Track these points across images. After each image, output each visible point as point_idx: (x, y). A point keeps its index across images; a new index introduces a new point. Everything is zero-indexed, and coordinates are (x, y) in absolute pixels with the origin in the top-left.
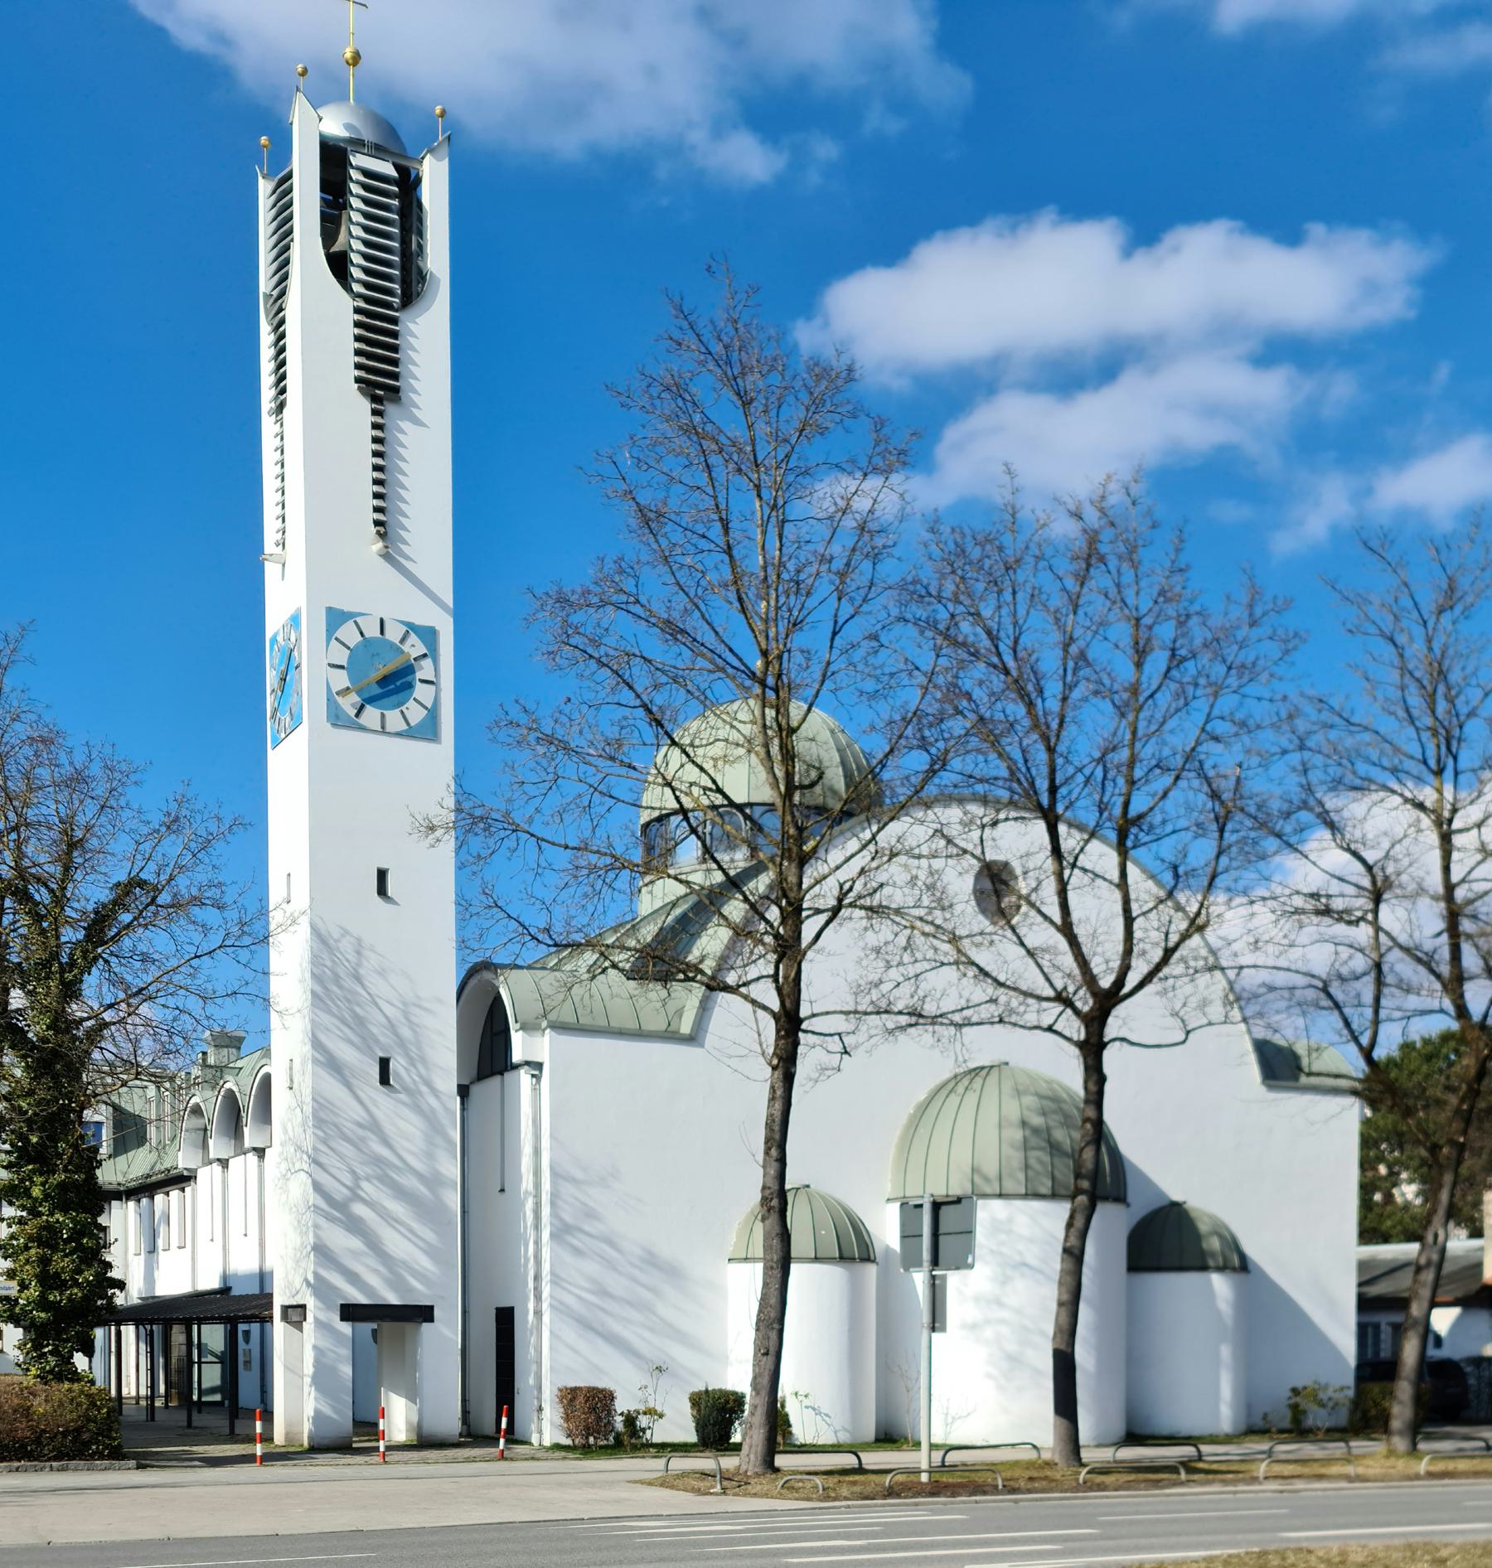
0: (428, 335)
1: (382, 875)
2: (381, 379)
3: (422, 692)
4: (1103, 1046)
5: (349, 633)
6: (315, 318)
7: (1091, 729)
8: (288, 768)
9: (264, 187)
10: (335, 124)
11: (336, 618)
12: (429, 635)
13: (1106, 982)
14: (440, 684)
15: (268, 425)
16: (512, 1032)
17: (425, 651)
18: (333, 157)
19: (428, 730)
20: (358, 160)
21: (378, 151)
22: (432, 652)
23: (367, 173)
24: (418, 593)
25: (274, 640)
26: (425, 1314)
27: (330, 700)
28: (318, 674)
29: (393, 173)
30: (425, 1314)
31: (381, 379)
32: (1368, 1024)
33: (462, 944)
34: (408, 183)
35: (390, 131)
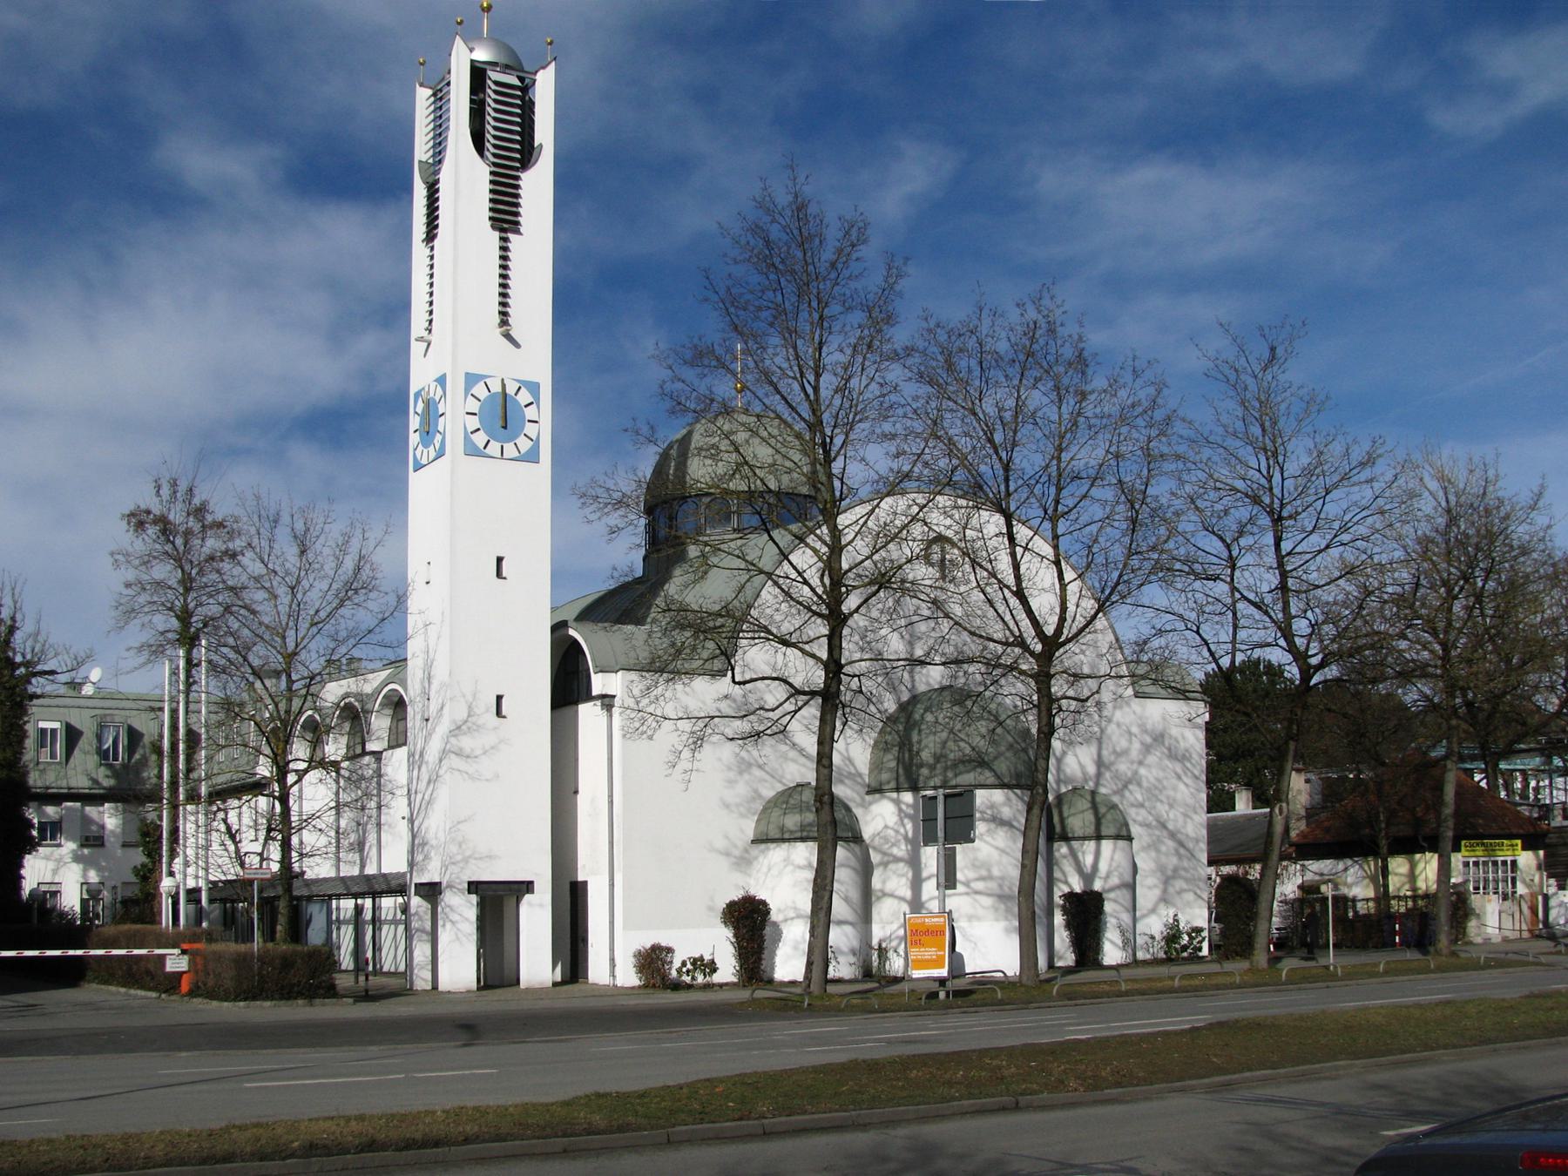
0: (537, 188)
1: (500, 560)
2: (505, 216)
3: (530, 429)
4: (1050, 677)
5: (480, 390)
6: (466, 177)
7: (1029, 459)
8: (428, 490)
9: (423, 95)
10: (482, 55)
11: (471, 379)
12: (534, 388)
13: (1049, 630)
14: (541, 421)
15: (419, 250)
16: (593, 675)
17: (531, 400)
18: (478, 74)
19: (532, 457)
20: (494, 75)
21: (507, 68)
22: (536, 401)
23: (497, 83)
24: (532, 360)
25: (418, 395)
26: (528, 887)
27: (466, 438)
28: (458, 416)
29: (518, 83)
30: (528, 887)
31: (505, 216)
32: (1404, 879)
33: (553, 610)
34: (526, 88)
35: (512, 53)
